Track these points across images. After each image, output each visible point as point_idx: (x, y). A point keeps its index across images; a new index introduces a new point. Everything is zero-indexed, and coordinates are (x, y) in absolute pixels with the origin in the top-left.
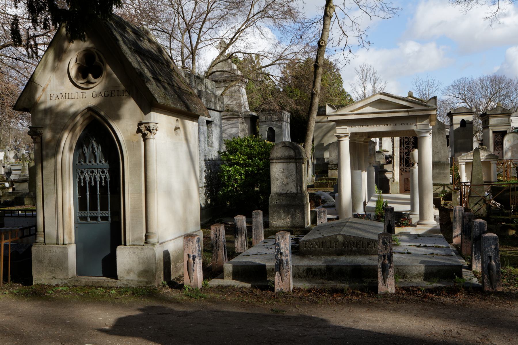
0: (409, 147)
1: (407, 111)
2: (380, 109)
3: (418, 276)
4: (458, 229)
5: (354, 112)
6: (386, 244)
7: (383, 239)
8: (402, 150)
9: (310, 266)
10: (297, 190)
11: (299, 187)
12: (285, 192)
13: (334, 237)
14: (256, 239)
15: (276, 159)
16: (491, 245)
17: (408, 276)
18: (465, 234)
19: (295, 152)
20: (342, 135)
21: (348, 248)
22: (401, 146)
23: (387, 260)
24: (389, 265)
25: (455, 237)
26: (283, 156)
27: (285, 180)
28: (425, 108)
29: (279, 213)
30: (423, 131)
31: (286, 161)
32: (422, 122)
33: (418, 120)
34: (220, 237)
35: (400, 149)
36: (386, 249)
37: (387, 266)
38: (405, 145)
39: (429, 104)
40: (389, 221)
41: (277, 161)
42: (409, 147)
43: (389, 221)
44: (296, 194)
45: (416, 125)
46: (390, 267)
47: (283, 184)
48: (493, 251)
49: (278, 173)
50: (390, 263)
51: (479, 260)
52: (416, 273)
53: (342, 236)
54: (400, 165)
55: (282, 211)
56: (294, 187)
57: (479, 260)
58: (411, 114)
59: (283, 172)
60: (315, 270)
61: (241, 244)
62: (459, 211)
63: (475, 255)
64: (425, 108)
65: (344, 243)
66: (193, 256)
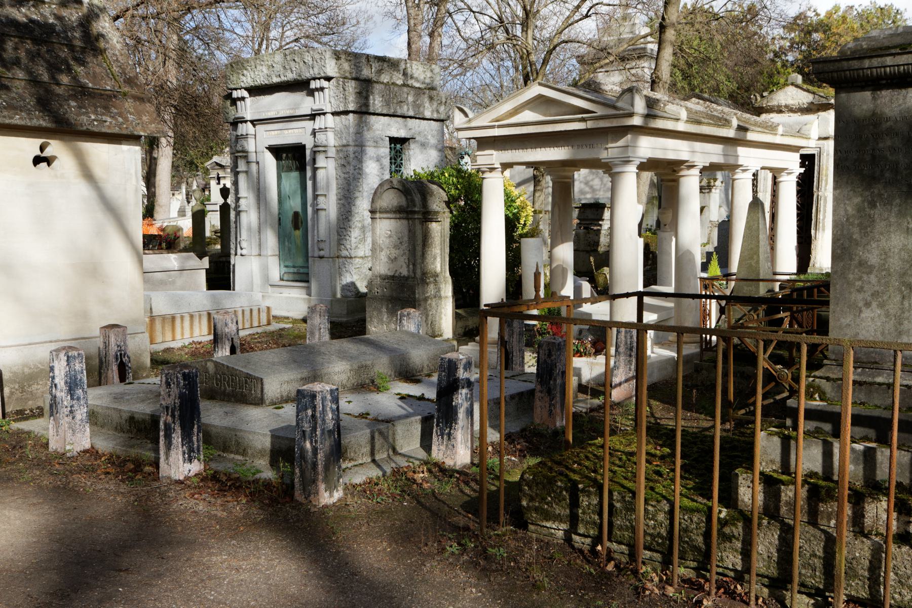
1: (583, 120)
2: (545, 115)
3: (261, 453)
4: (621, 370)
5: (497, 124)
7: (167, 375)
9: (133, 413)
10: (409, 271)
11: (411, 266)
15: (380, 212)
16: (306, 409)
17: (250, 452)
18: (541, 382)
19: (407, 199)
20: (484, 168)
25: (616, 386)
26: (390, 206)
27: (393, 251)
28: (613, 112)
29: (380, 312)
30: (616, 161)
31: (398, 216)
32: (617, 141)
39: (619, 104)
41: (382, 216)
44: (406, 278)
45: (607, 149)
47: (389, 258)
49: (383, 238)
51: (442, 438)
52: (260, 447)
55: (384, 310)
56: (405, 266)
57: (442, 438)
59: (390, 236)
60: (138, 422)
63: (438, 425)
64: (613, 112)
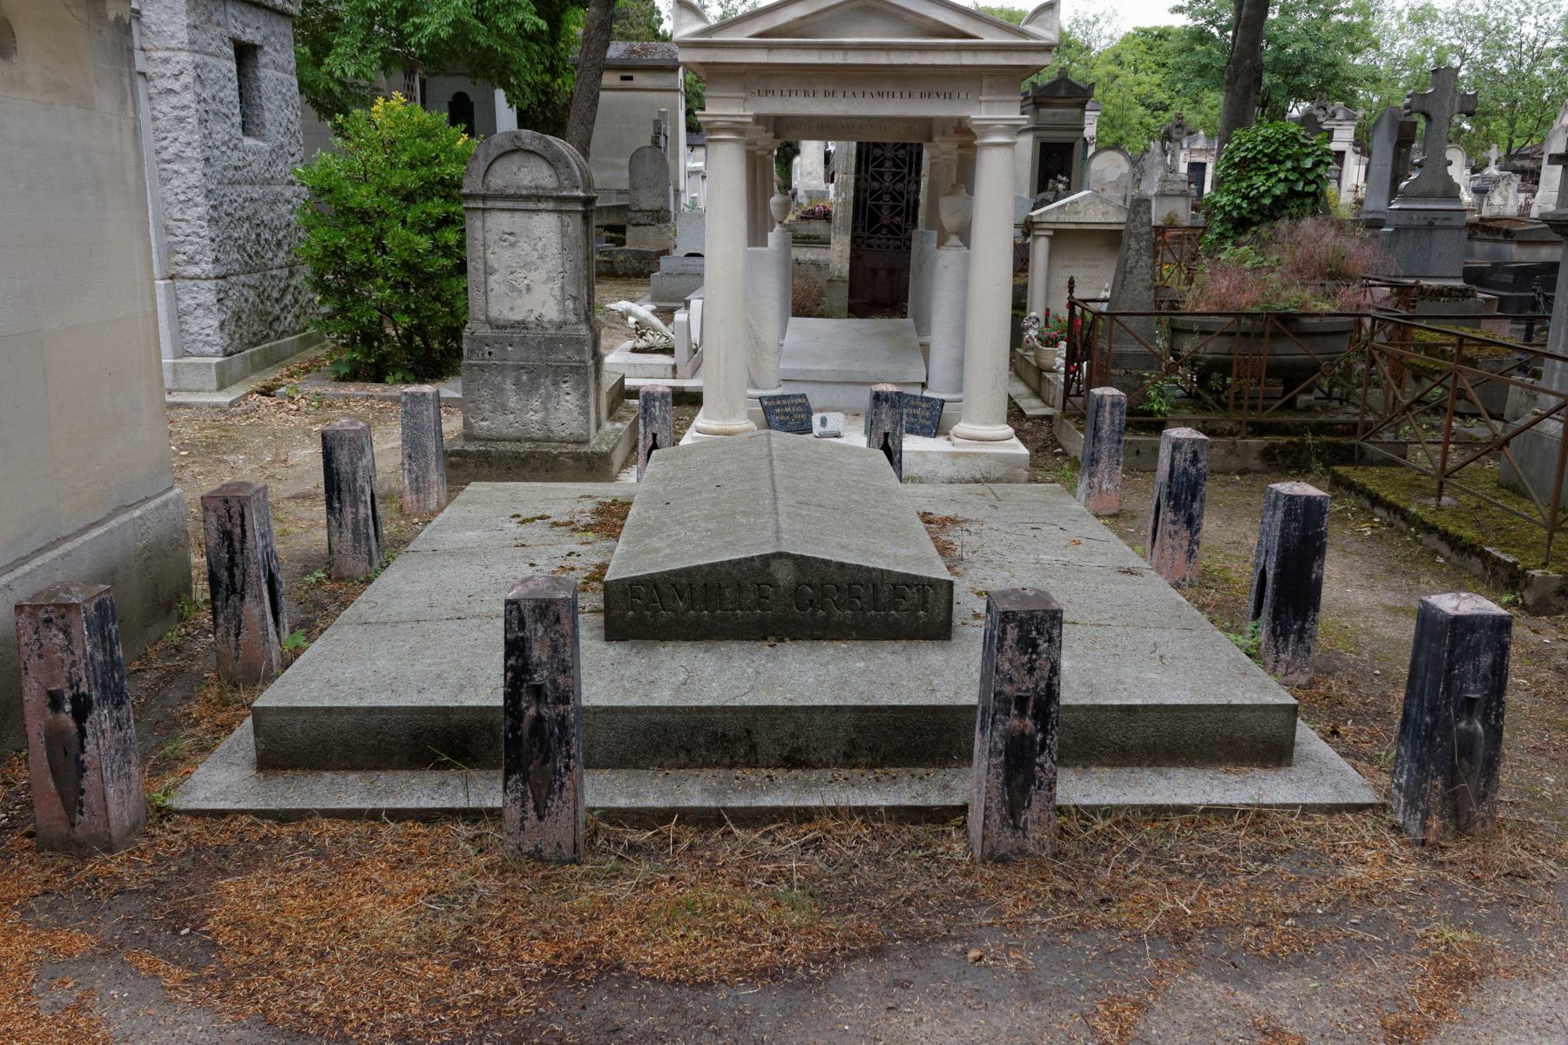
0: (881, 174)
6: (1035, 646)
8: (863, 184)
12: (519, 317)
13: (757, 564)
14: (418, 491)
21: (813, 614)
22: (858, 171)
23: (1035, 717)
24: (1039, 737)
33: (985, 82)
34: (250, 543)
35: (857, 180)
36: (1031, 671)
37: (1033, 742)
38: (871, 169)
39: (1030, 28)
40: (886, 435)
42: (881, 174)
43: (886, 435)
46: (1043, 745)
48: (1485, 678)
50: (1044, 730)
53: (790, 563)
54: (854, 229)
57: (1286, 640)
58: (967, 59)
61: (355, 530)
62: (1113, 405)
65: (796, 592)
66: (75, 700)
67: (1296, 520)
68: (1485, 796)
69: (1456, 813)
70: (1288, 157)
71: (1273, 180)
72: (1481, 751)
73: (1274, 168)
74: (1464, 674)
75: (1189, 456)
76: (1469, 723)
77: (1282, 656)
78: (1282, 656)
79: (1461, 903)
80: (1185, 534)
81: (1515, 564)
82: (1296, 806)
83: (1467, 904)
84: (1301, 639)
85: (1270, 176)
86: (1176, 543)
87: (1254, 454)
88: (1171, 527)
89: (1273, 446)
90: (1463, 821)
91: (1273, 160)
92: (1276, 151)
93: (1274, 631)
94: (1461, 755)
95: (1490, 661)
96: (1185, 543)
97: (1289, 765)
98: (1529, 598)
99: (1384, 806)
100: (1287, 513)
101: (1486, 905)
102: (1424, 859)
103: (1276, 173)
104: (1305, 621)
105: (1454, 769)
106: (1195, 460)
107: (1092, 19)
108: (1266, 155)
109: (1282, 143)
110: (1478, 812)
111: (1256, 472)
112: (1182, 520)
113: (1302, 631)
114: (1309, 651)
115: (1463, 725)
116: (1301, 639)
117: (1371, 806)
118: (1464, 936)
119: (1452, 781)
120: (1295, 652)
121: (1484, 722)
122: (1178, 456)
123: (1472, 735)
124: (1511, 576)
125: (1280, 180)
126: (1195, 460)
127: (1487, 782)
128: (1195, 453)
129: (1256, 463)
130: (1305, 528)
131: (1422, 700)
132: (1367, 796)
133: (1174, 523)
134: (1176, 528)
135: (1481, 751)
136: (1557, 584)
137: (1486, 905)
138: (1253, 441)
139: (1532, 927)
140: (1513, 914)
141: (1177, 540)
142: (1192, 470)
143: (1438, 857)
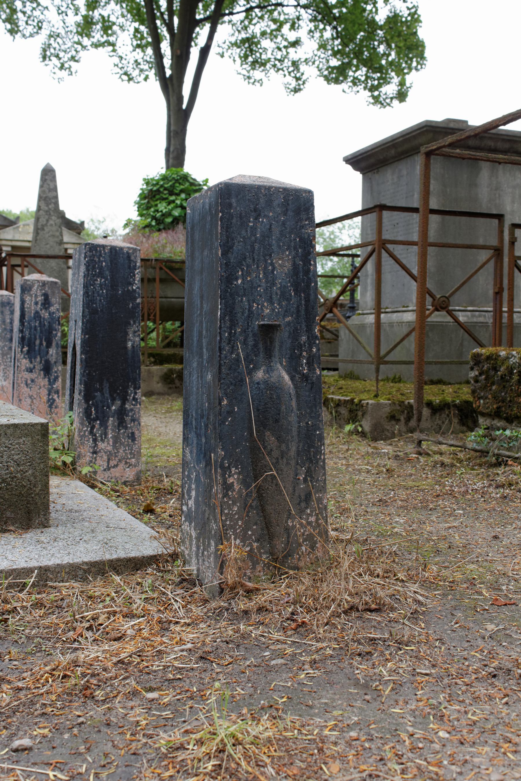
48: (284, 295)
57: (104, 424)
67: (101, 275)
68: (308, 497)
69: (267, 533)
70: (182, 191)
71: (172, 205)
72: (293, 418)
73: (172, 198)
74: (253, 287)
75: (40, 299)
76: (269, 370)
77: (101, 445)
78: (101, 445)
79: (269, 669)
80: (43, 382)
81: (352, 400)
82: (28, 571)
83: (276, 669)
84: (121, 423)
85: (169, 203)
86: (34, 392)
87: (156, 379)
88: (28, 376)
89: (171, 371)
90: (280, 545)
91: (171, 193)
92: (173, 186)
93: (87, 413)
94: (262, 424)
95: (288, 265)
96: (44, 392)
97: (45, 525)
98: (366, 425)
99: (174, 556)
100: (91, 265)
101: (313, 663)
102: (219, 613)
103: (173, 201)
104: (124, 400)
105: (254, 452)
106: (46, 303)
107: (102, 220)
108: (165, 189)
109: (177, 181)
110: (299, 525)
111: (159, 394)
112: (39, 367)
113: (121, 414)
114: (133, 437)
115: (260, 374)
116: (121, 423)
117: (152, 560)
118: (264, 728)
119: (254, 470)
120: (116, 439)
121: (293, 369)
122: (28, 299)
123: (273, 389)
124: (351, 411)
125: (177, 207)
126: (46, 303)
127: (309, 473)
128: (46, 296)
129: (158, 386)
130: (114, 286)
131: (201, 355)
132: (149, 548)
133: (31, 371)
134: (33, 376)
135: (293, 418)
136: (388, 409)
137: (313, 663)
138: (155, 368)
139: (397, 686)
140: (361, 669)
141: (35, 389)
142: (45, 314)
143: (242, 604)
